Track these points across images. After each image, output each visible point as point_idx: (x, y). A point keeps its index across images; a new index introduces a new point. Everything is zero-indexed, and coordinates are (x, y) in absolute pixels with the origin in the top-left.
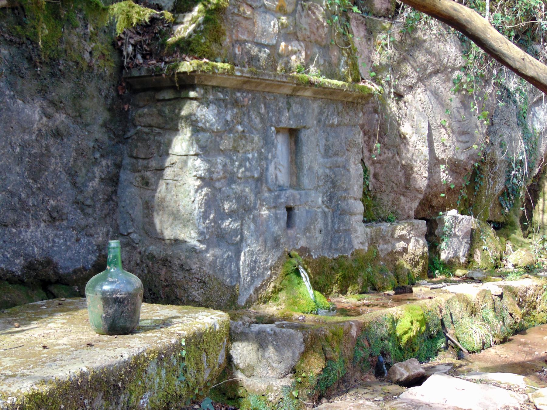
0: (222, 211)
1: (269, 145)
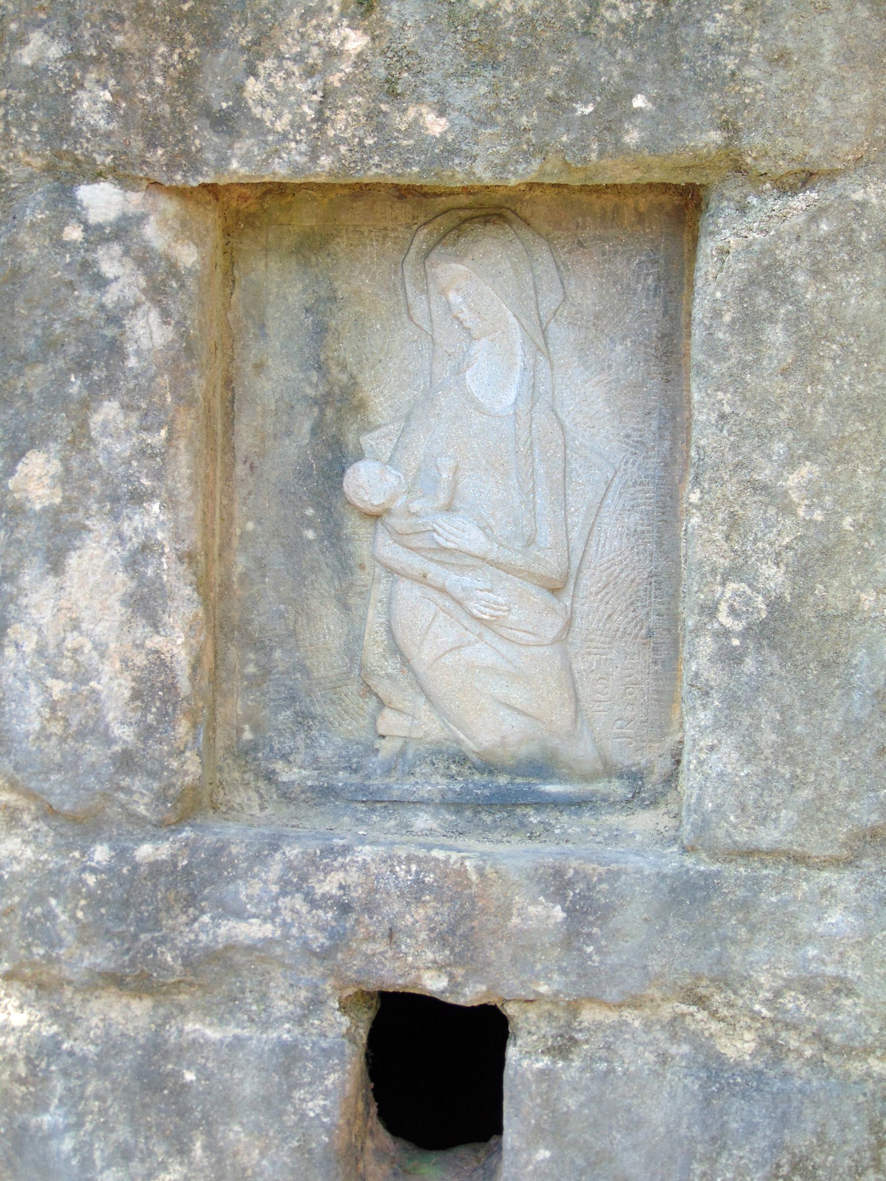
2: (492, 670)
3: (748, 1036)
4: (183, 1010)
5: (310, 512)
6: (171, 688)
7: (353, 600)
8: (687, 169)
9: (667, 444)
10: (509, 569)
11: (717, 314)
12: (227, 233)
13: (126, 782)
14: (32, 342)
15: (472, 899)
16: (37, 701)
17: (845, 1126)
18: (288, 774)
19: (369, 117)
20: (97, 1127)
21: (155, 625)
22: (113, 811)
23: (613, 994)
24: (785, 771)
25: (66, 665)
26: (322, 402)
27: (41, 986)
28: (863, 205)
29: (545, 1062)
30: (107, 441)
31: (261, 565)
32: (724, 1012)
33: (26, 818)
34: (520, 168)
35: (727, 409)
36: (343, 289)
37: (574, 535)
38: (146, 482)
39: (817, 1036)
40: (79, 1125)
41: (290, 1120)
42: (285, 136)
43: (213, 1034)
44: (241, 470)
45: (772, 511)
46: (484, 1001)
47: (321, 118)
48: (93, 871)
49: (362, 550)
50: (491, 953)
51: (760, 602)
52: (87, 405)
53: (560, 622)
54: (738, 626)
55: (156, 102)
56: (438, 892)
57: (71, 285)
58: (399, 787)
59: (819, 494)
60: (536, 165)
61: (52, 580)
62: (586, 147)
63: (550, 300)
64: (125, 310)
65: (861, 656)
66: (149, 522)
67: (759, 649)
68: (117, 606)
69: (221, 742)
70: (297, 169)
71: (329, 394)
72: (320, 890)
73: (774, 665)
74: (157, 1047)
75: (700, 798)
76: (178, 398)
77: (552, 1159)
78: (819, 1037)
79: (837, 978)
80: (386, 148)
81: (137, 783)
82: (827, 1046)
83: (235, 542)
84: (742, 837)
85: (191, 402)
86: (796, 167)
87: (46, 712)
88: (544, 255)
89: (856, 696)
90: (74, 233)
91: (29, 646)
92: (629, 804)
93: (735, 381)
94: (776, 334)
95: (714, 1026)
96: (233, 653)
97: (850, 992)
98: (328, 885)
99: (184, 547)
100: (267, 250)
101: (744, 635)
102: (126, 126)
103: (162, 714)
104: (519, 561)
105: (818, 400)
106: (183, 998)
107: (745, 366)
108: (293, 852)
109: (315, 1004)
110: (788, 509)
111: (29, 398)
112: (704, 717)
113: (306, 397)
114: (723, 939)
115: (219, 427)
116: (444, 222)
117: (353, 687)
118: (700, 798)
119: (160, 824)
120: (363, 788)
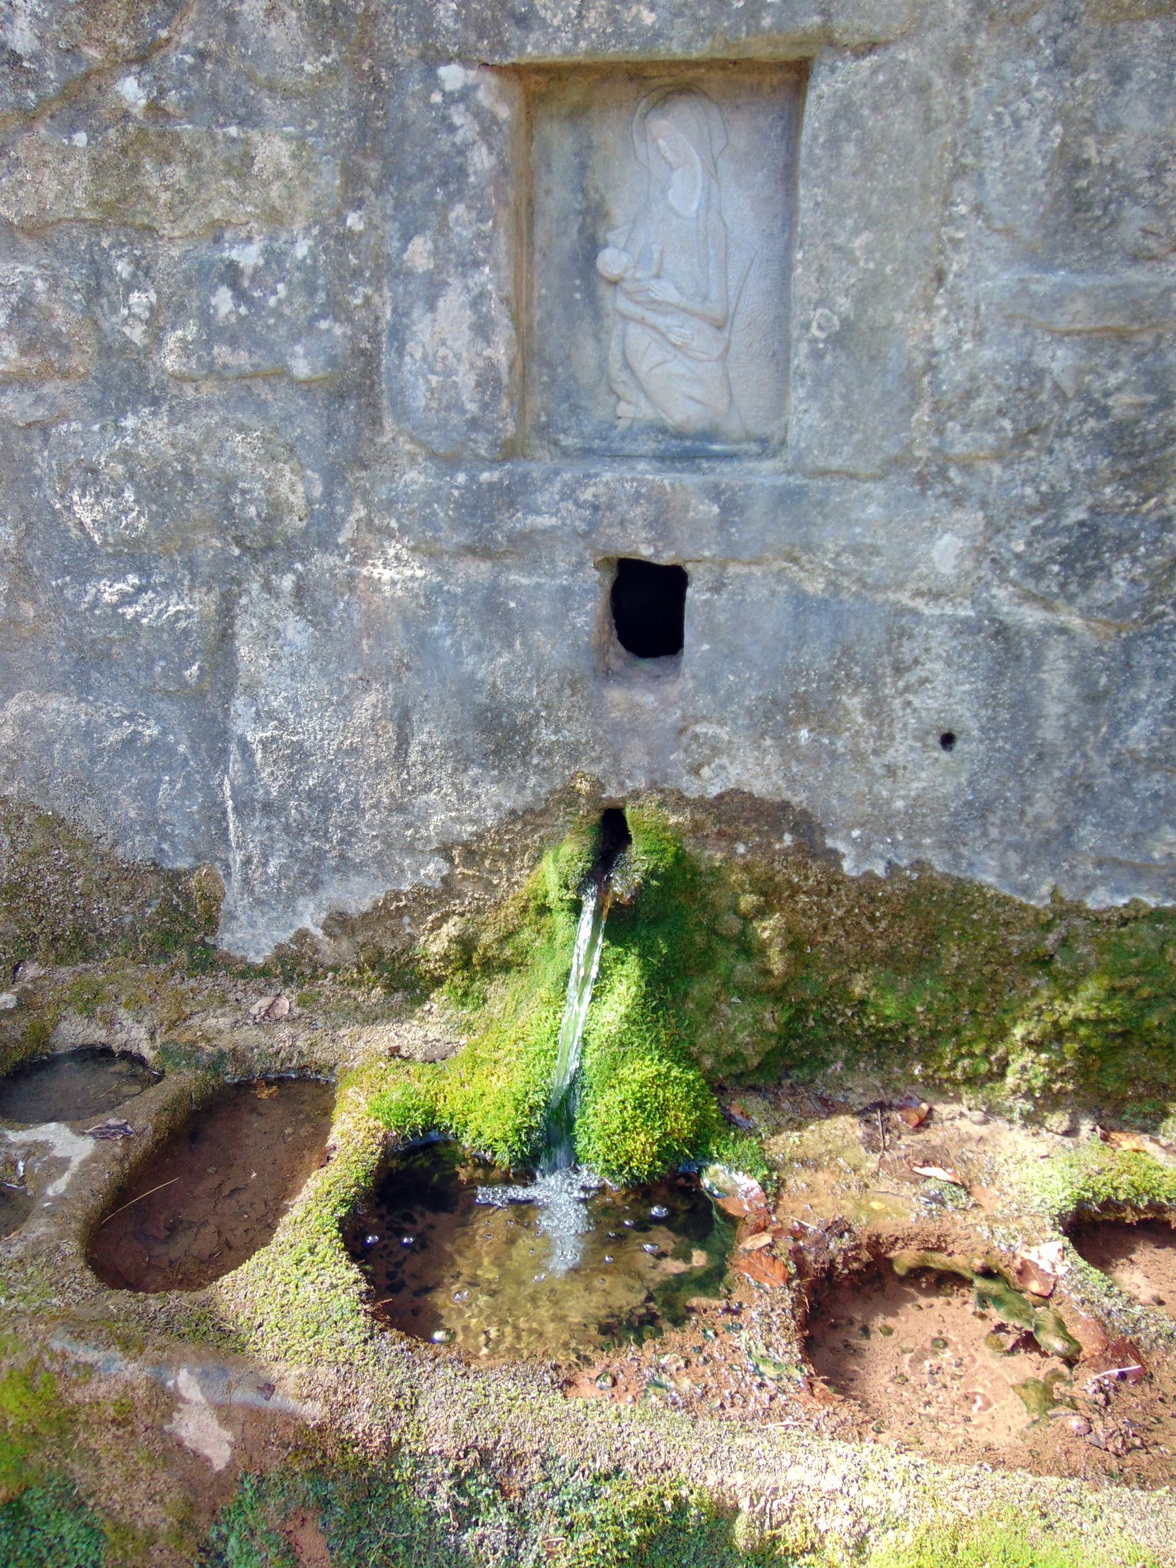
0: (74, 533)
1: (418, 190)
2: (682, 377)
3: (821, 580)
4: (508, 568)
5: (578, 282)
6: (498, 380)
7: (603, 336)
8: (800, 44)
9: (786, 235)
10: (694, 314)
11: (815, 137)
12: (528, 105)
13: (473, 436)
14: (414, 168)
15: (667, 502)
16: (423, 388)
17: (872, 630)
18: (567, 441)
19: (609, 14)
20: (464, 632)
21: (488, 342)
22: (467, 454)
23: (745, 556)
24: (847, 423)
25: (439, 367)
26: (584, 213)
27: (431, 555)
28: (905, 62)
29: (707, 596)
30: (458, 229)
31: (550, 316)
32: (808, 566)
33: (420, 459)
34: (700, 45)
35: (820, 199)
36: (596, 140)
37: (731, 293)
38: (481, 254)
39: (859, 579)
40: (454, 632)
41: (568, 628)
42: (558, 29)
43: (525, 581)
44: (538, 257)
45: (844, 263)
46: (674, 562)
47: (580, 16)
48: (457, 488)
49: (608, 306)
50: (678, 533)
51: (836, 320)
52: (447, 206)
53: (722, 347)
54: (823, 336)
55: (482, 10)
56: (648, 499)
57: (436, 131)
58: (629, 447)
59: (872, 252)
60: (708, 42)
61: (429, 316)
62: (738, 30)
63: (719, 144)
64: (468, 145)
65: (893, 352)
66: (483, 279)
67: (834, 349)
68: (467, 332)
69: (529, 421)
70: (566, 52)
71: (588, 208)
72: (582, 498)
73: (843, 359)
74: (494, 589)
75: (798, 441)
76: (498, 201)
77: (711, 650)
78: (860, 580)
79: (872, 546)
80: (619, 34)
81: (480, 436)
82: (864, 585)
83: (535, 302)
84: (821, 464)
85: (506, 204)
86: (865, 39)
87: (428, 395)
88: (715, 113)
89: (889, 376)
90: (437, 98)
91: (418, 355)
92: (759, 456)
93: (825, 180)
94: (850, 149)
95: (802, 575)
96: (535, 369)
97: (878, 554)
98: (587, 495)
99: (504, 294)
100: (551, 117)
101: (826, 341)
102: (465, 27)
103: (493, 395)
104: (697, 307)
105: (873, 191)
106: (508, 561)
107: (831, 170)
108: (567, 476)
109: (580, 564)
110: (853, 262)
111: (414, 203)
112: (801, 392)
113: (575, 210)
114: (808, 524)
115: (525, 228)
116: (655, 96)
117: (603, 389)
118: (798, 441)
119: (493, 461)
120: (609, 449)
